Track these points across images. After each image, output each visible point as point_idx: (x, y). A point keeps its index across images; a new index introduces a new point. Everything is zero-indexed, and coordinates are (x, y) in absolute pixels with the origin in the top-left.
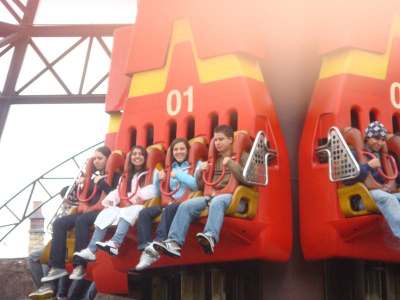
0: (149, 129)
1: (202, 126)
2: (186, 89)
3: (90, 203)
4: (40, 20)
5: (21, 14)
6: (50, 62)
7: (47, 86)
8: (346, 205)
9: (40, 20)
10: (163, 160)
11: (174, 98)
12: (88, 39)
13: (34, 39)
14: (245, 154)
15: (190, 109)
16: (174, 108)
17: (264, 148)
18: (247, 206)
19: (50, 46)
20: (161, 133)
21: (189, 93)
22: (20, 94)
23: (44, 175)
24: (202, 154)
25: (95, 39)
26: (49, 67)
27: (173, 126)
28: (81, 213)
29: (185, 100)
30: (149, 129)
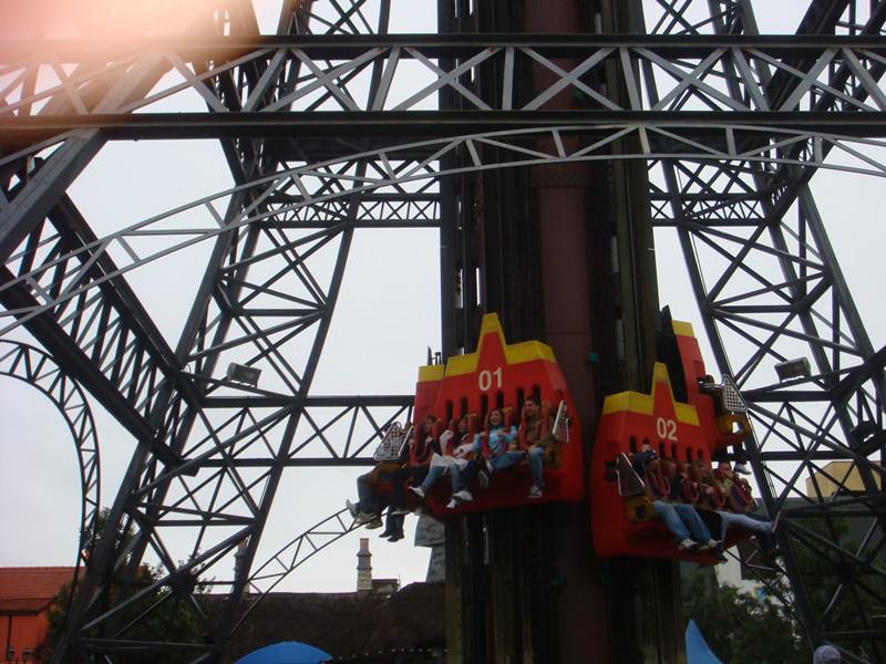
0: (464, 402)
1: (510, 398)
2: (495, 370)
3: (420, 461)
4: (313, 392)
5: (297, 387)
6: (320, 428)
7: (317, 450)
8: (632, 514)
9: (313, 392)
10: (481, 425)
11: (485, 377)
12: (354, 409)
13: (306, 408)
14: (551, 418)
15: (499, 385)
16: (485, 384)
17: (565, 414)
18: (554, 459)
19: (321, 415)
20: (474, 404)
21: (498, 372)
22: (293, 457)
23: (393, 419)
24: (515, 421)
25: (360, 409)
26: (319, 433)
27: (484, 397)
28: (413, 468)
29: (495, 378)
30: (464, 402)
